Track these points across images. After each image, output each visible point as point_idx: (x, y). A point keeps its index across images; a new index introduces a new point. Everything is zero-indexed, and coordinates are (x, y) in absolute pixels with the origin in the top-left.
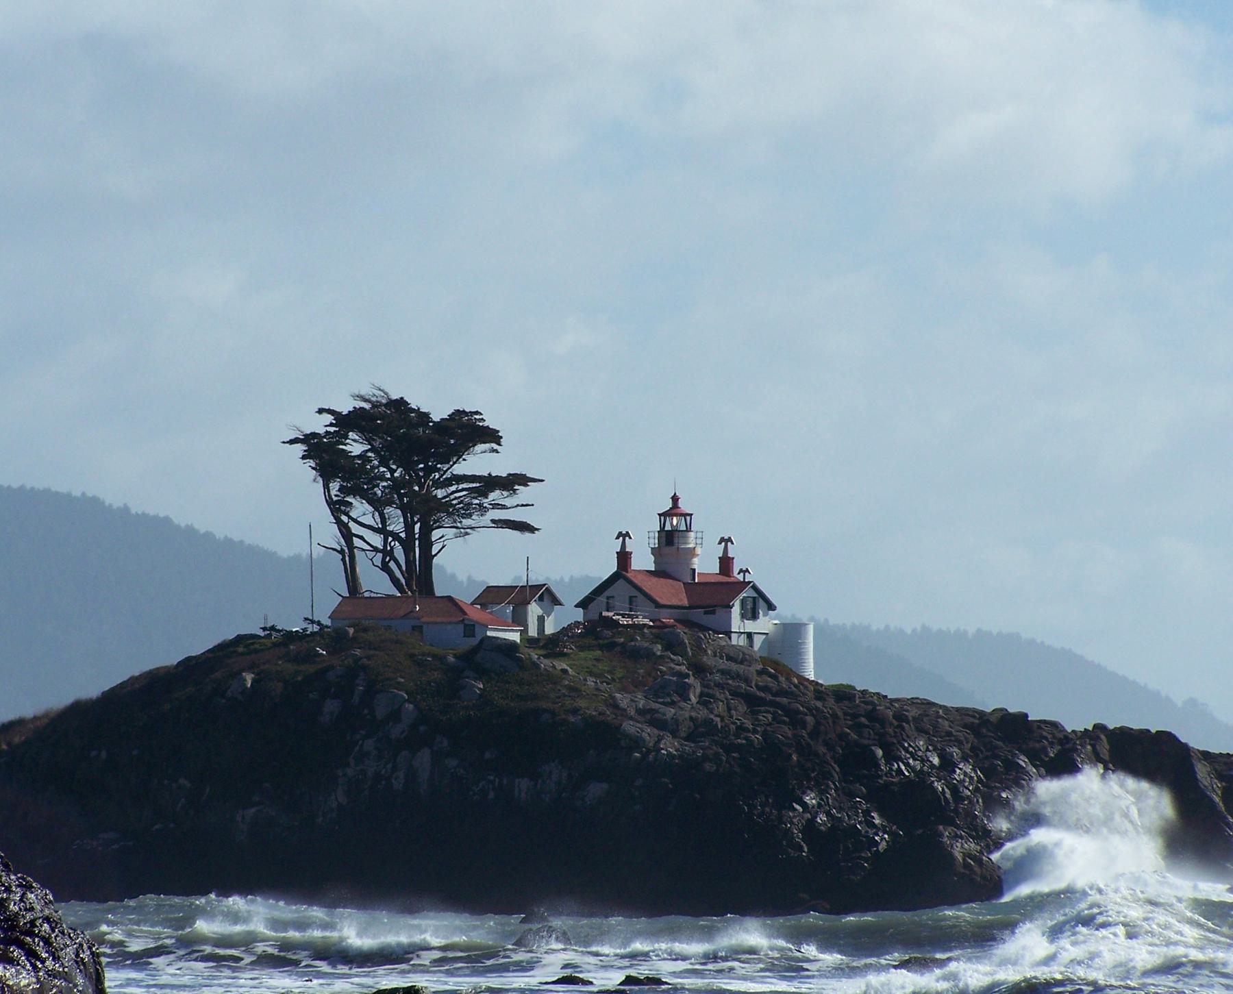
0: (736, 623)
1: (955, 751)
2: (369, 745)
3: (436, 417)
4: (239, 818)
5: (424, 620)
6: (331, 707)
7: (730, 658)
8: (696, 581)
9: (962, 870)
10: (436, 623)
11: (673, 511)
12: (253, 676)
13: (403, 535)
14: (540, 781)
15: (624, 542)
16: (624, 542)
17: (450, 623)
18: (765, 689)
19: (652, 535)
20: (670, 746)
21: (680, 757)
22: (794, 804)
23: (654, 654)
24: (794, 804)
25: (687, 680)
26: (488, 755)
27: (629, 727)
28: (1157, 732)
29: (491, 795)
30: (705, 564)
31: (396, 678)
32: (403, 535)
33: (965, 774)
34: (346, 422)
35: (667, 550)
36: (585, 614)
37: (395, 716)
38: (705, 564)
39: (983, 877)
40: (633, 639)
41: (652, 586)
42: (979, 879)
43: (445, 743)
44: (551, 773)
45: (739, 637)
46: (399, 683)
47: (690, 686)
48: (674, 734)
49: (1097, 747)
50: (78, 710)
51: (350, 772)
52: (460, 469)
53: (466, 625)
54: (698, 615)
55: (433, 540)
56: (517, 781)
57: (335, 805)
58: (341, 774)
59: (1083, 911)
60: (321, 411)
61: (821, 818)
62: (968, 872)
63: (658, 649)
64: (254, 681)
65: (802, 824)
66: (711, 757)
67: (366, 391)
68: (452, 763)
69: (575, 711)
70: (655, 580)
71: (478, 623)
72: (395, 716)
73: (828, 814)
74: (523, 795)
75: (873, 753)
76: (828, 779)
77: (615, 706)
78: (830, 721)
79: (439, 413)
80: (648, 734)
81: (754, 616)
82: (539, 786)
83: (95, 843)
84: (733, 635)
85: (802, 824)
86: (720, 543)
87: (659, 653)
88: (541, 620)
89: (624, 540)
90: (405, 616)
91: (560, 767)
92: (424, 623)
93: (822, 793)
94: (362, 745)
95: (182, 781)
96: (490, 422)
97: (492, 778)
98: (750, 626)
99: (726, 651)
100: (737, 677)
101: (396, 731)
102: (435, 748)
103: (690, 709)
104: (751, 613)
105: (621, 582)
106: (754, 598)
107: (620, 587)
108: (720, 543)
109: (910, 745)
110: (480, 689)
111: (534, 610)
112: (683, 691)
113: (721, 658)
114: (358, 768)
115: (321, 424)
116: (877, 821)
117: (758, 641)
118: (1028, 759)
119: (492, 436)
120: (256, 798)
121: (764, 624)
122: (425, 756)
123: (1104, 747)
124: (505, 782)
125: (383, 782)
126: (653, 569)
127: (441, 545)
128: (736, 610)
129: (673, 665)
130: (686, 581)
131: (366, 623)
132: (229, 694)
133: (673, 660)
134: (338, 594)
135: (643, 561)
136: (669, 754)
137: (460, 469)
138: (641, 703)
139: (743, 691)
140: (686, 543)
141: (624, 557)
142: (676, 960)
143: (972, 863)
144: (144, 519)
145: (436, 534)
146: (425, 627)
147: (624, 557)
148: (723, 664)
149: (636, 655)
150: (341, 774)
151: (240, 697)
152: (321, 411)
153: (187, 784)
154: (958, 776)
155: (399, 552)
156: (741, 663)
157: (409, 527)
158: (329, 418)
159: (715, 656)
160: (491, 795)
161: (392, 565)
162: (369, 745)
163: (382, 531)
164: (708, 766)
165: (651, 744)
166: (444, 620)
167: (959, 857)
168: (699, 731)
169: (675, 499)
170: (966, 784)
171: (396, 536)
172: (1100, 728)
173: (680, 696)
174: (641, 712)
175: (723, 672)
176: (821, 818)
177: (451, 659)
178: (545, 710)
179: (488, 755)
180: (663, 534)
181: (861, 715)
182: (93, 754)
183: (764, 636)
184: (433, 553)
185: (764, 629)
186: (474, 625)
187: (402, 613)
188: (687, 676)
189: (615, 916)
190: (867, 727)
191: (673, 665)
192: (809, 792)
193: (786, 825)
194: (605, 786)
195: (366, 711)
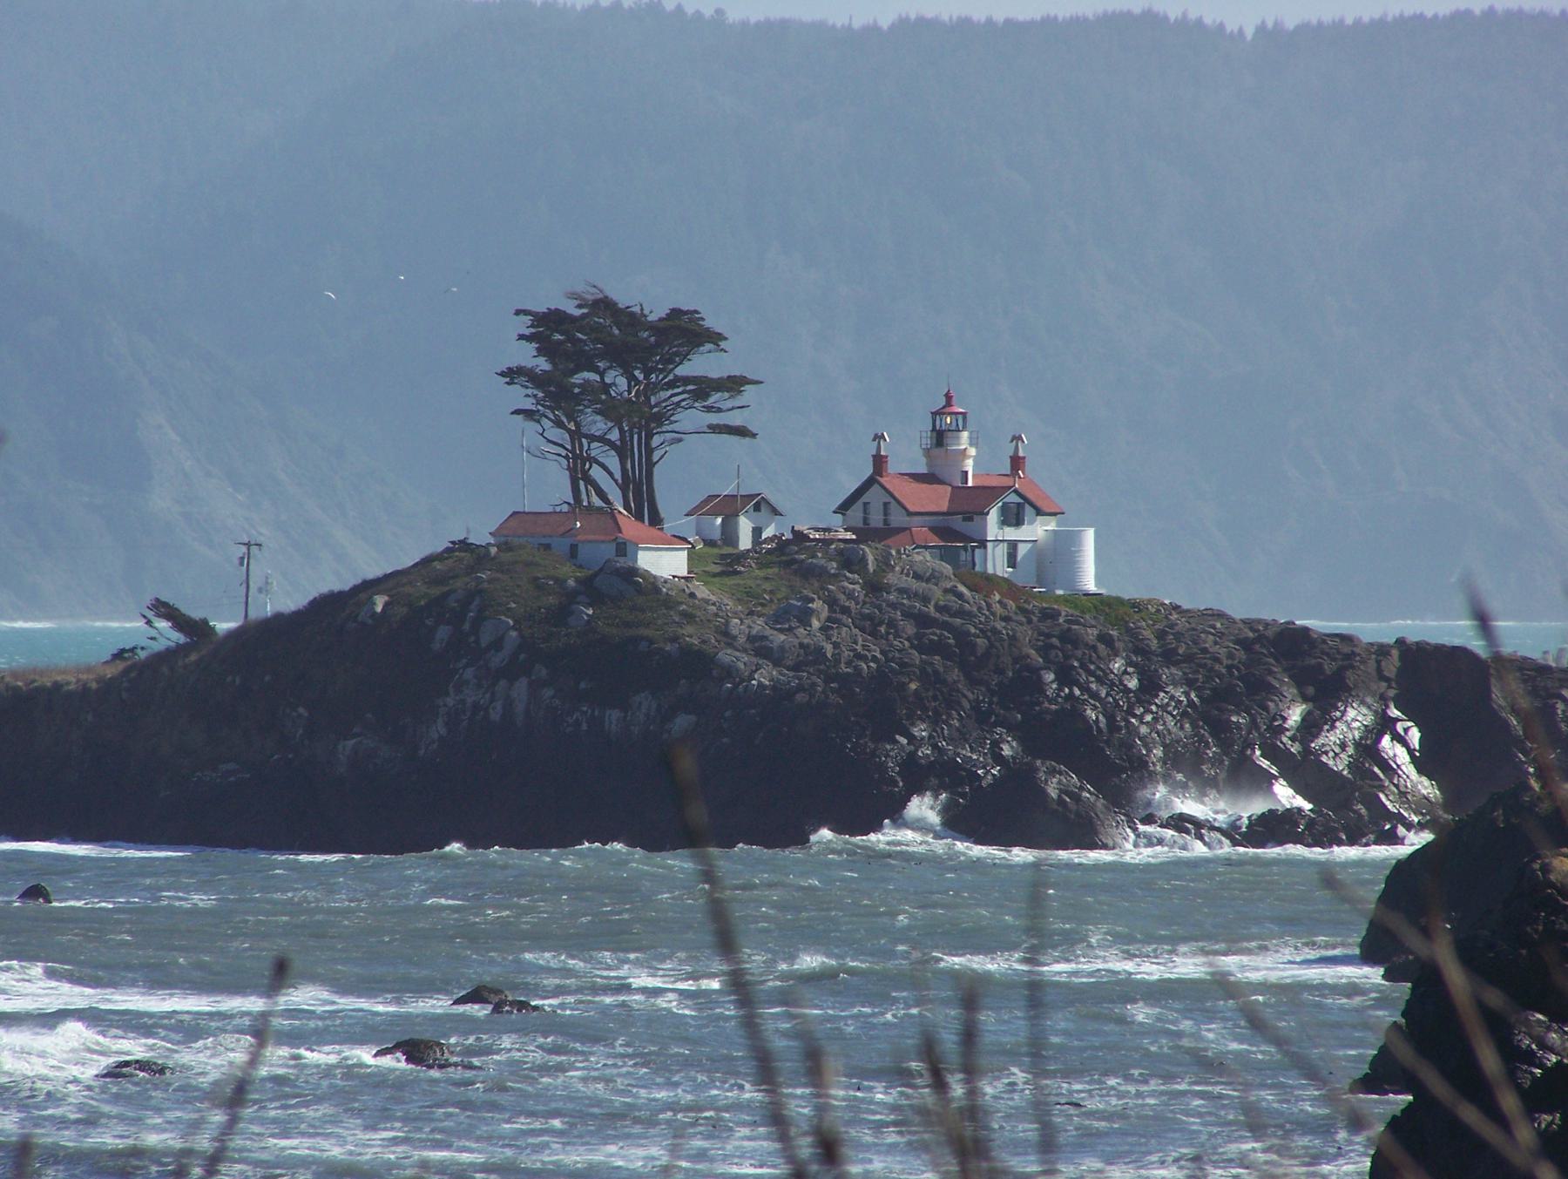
2: (469, 673)
3: (652, 318)
4: (340, 747)
5: (579, 538)
6: (443, 632)
7: (917, 576)
8: (970, 484)
9: (1055, 807)
10: (590, 542)
11: (947, 410)
12: (386, 598)
13: (618, 443)
14: (629, 714)
17: (603, 542)
19: (924, 434)
20: (764, 676)
21: (774, 688)
22: (897, 737)
23: (828, 572)
24: (897, 737)
25: (810, 605)
26: (583, 685)
29: (584, 727)
31: (508, 603)
32: (618, 443)
33: (1172, 698)
35: (937, 451)
36: (844, 520)
37: (497, 644)
39: (1078, 814)
40: (814, 556)
42: (1073, 816)
44: (640, 703)
45: (994, 547)
46: (509, 609)
47: (812, 611)
48: (777, 663)
49: (1383, 664)
51: (450, 701)
52: (683, 370)
53: (618, 544)
54: (957, 523)
55: (653, 446)
56: (608, 713)
57: (436, 736)
58: (441, 704)
60: (518, 312)
62: (1060, 809)
64: (386, 605)
65: (902, 757)
66: (806, 687)
68: (548, 693)
69: (674, 639)
70: (915, 485)
71: (631, 542)
72: (497, 644)
73: (935, 747)
76: (952, 708)
78: (1006, 644)
82: (628, 718)
83: (214, 775)
84: (990, 545)
85: (902, 757)
86: (1012, 441)
87: (833, 571)
88: (757, 532)
89: (879, 443)
90: (563, 535)
91: (650, 697)
92: (579, 541)
93: (935, 722)
94: (462, 674)
95: (301, 710)
96: (711, 322)
97: (585, 709)
98: (1011, 533)
99: (915, 568)
101: (497, 660)
102: (533, 678)
104: (1013, 517)
105: (876, 487)
106: (1019, 504)
108: (1012, 441)
109: (1099, 668)
110: (588, 615)
111: (745, 526)
112: (804, 617)
113: (908, 575)
114: (457, 698)
117: (1022, 550)
119: (716, 338)
121: (1037, 530)
122: (521, 688)
124: (596, 713)
125: (482, 713)
126: (925, 471)
127: (663, 452)
128: (993, 516)
129: (846, 584)
130: (955, 484)
131: (516, 541)
132: (360, 618)
133: (848, 579)
135: (907, 455)
136: (760, 684)
137: (683, 370)
139: (916, 611)
140: (959, 444)
141: (879, 461)
143: (1068, 800)
145: (656, 441)
146: (580, 545)
147: (879, 461)
150: (441, 704)
151: (370, 621)
152: (518, 312)
156: (928, 581)
158: (527, 319)
159: (902, 572)
160: (584, 727)
162: (469, 673)
164: (801, 698)
165: (746, 674)
166: (602, 538)
167: (1053, 793)
168: (812, 656)
169: (948, 397)
170: (1170, 709)
173: (800, 621)
175: (901, 591)
177: (571, 582)
178: (642, 638)
179: (583, 685)
180: (935, 434)
181: (1054, 636)
182: (229, 679)
183: (1030, 545)
184: (655, 460)
185: (1032, 536)
186: (625, 544)
187: (562, 529)
188: (812, 600)
189: (1340, 843)
190: (1057, 648)
191: (846, 584)
192: (918, 722)
193: (880, 759)
194: (693, 718)
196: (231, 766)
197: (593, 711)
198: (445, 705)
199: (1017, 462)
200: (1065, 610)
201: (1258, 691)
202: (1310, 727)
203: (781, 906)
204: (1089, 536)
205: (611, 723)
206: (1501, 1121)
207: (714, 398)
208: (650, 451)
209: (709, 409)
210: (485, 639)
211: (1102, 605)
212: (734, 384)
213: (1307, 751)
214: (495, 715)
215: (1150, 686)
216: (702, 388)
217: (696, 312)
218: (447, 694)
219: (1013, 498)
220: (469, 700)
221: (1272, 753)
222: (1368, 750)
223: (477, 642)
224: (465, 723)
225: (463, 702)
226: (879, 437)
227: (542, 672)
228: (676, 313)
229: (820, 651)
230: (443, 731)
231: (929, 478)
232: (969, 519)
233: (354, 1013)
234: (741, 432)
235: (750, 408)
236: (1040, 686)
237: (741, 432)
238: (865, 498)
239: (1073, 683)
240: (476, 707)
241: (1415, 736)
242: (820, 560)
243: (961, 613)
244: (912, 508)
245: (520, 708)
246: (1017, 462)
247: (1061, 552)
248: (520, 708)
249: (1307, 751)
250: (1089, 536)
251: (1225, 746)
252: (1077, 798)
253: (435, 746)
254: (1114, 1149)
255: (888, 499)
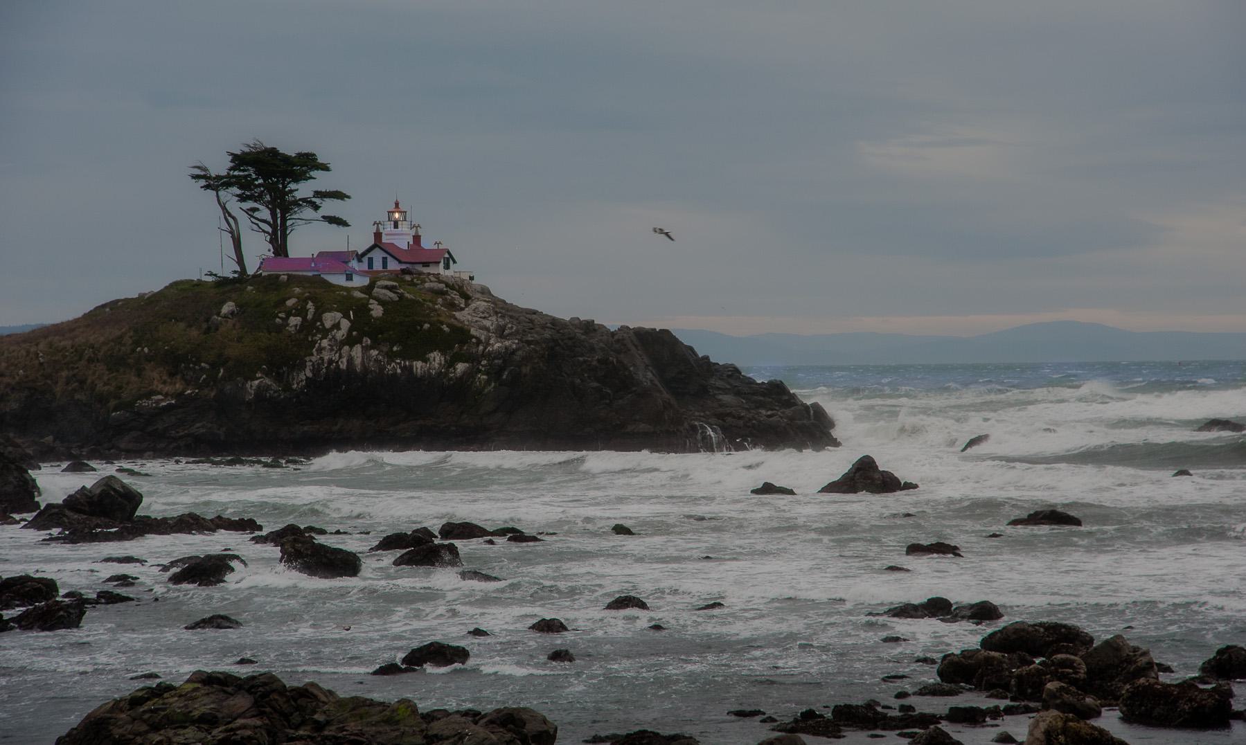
4: (248, 386)
6: (295, 321)
15: (417, 230)
16: (417, 230)
26: (395, 349)
28: (660, 330)
37: (337, 326)
43: (369, 342)
51: (314, 359)
57: (304, 378)
68: (374, 353)
74: (419, 370)
94: (320, 344)
95: (203, 364)
97: (398, 361)
101: (340, 334)
105: (377, 250)
120: (258, 375)
122: (357, 351)
134: (1001, 458)
142: (212, 618)
147: (378, 235)
153: (207, 366)
154: (155, 375)
160: (399, 371)
162: (325, 343)
179: (395, 349)
194: (467, 365)
195: (319, 323)
196: (160, 397)
197: (405, 362)
198: (311, 361)
205: (417, 368)
206: (229, 599)
208: (286, 228)
210: (328, 325)
214: (343, 366)
217: (314, 155)
218: (312, 355)
220: (326, 358)
223: (323, 324)
224: (324, 370)
225: (322, 359)
227: (367, 341)
230: (309, 374)
238: (369, 255)
240: (330, 362)
244: (403, 260)
245: (358, 361)
248: (358, 361)
253: (304, 383)
254: (1023, 577)
255: (385, 255)
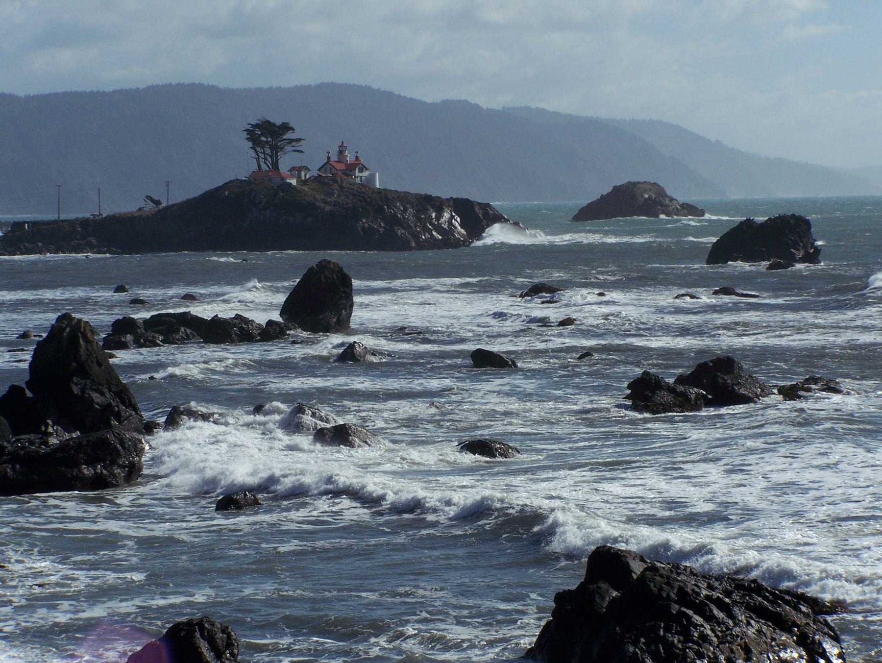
0: (357, 174)
1: (408, 206)
3: (278, 124)
18: (359, 192)
20: (328, 208)
27: (318, 204)
30: (350, 157)
34: (256, 126)
38: (350, 157)
41: (335, 164)
48: (330, 205)
50: (195, 198)
52: (285, 137)
54: (348, 172)
59: (263, 287)
61: (366, 225)
63: (331, 182)
67: (260, 118)
75: (384, 208)
77: (315, 198)
79: (278, 123)
80: (322, 205)
81: (362, 172)
88: (305, 175)
93: (367, 219)
96: (291, 125)
98: (361, 174)
100: (351, 189)
103: (335, 198)
104: (361, 171)
107: (328, 166)
111: (303, 173)
112: (333, 194)
115: (249, 127)
116: (382, 225)
117: (363, 178)
118: (221, 262)
119: (293, 129)
121: (366, 174)
123: (451, 203)
135: (334, 158)
137: (285, 137)
138: (322, 197)
141: (329, 158)
144: (385, 92)
147: (329, 158)
148: (348, 186)
149: (325, 184)
155: (270, 159)
157: (272, 152)
161: (267, 162)
163: (264, 153)
167: (399, 234)
168: (336, 204)
171: (268, 155)
172: (451, 198)
174: (322, 200)
175: (348, 188)
176: (366, 225)
199: (357, 158)
200: (383, 192)
201: (425, 211)
202: (438, 218)
203: (811, 292)
204: (377, 174)
207: (294, 143)
209: (293, 146)
211: (379, 192)
212: (298, 140)
213: (438, 223)
215: (405, 209)
216: (291, 141)
219: (361, 166)
221: (432, 224)
222: (450, 223)
226: (357, 152)
228: (284, 123)
229: (339, 202)
231: (338, 162)
232: (351, 171)
233: (755, 332)
234: (301, 152)
235: (303, 145)
236: (384, 209)
237: (301, 152)
239: (391, 209)
241: (459, 219)
242: (327, 180)
243: (364, 193)
246: (357, 158)
247: (372, 178)
249: (438, 223)
250: (377, 174)
251: (421, 223)
252: (404, 235)
